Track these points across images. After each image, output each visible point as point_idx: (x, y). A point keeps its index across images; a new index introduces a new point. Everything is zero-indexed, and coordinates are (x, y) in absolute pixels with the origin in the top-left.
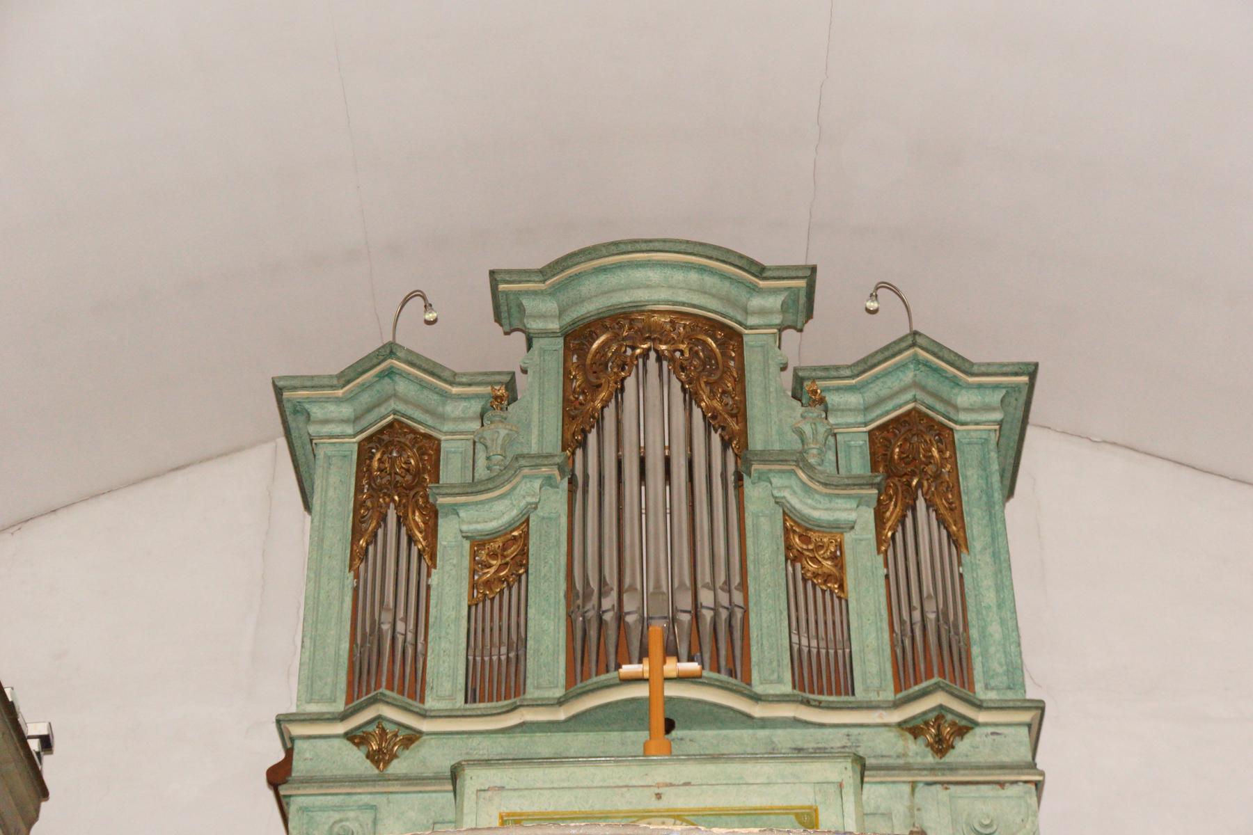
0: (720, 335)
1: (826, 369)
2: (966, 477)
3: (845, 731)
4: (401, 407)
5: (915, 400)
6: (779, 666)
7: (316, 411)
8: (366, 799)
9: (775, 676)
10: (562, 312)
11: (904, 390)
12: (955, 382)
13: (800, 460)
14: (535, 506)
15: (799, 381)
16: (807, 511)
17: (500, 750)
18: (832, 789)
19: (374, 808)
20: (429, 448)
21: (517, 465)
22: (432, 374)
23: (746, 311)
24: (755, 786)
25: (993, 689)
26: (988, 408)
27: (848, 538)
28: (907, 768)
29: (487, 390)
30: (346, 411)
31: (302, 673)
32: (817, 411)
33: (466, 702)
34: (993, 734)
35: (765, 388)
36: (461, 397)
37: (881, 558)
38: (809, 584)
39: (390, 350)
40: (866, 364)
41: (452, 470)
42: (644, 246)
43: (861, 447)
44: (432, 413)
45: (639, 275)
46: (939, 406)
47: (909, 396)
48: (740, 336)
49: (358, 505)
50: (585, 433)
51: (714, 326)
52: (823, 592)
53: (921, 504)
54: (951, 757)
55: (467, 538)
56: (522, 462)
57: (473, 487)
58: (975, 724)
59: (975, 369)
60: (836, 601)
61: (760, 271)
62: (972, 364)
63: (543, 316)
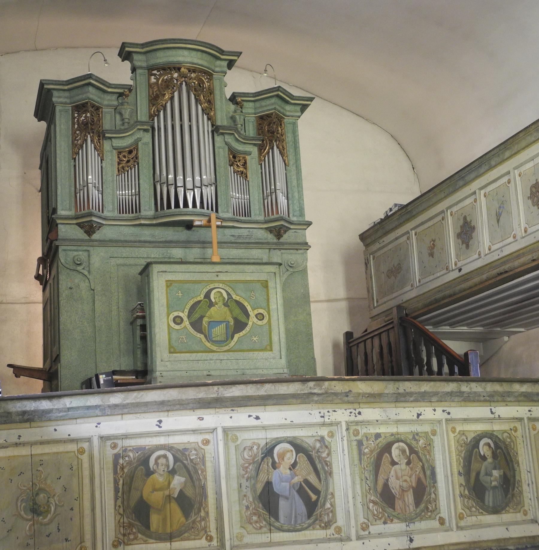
2: (288, 137)
3: (248, 230)
6: (227, 206)
8: (85, 248)
9: (226, 210)
17: (131, 232)
18: (273, 274)
19: (88, 251)
21: (136, 124)
23: (216, 67)
24: (276, 296)
25: (295, 216)
27: (248, 158)
28: (268, 243)
33: (120, 213)
34: (295, 232)
35: (221, 97)
37: (260, 166)
38: (236, 174)
42: (184, 42)
43: (253, 122)
50: (159, 111)
52: (240, 177)
53: (275, 147)
54: (282, 240)
55: (115, 149)
56: (138, 123)
58: (290, 229)
59: (294, 98)
60: (244, 181)
62: (293, 96)
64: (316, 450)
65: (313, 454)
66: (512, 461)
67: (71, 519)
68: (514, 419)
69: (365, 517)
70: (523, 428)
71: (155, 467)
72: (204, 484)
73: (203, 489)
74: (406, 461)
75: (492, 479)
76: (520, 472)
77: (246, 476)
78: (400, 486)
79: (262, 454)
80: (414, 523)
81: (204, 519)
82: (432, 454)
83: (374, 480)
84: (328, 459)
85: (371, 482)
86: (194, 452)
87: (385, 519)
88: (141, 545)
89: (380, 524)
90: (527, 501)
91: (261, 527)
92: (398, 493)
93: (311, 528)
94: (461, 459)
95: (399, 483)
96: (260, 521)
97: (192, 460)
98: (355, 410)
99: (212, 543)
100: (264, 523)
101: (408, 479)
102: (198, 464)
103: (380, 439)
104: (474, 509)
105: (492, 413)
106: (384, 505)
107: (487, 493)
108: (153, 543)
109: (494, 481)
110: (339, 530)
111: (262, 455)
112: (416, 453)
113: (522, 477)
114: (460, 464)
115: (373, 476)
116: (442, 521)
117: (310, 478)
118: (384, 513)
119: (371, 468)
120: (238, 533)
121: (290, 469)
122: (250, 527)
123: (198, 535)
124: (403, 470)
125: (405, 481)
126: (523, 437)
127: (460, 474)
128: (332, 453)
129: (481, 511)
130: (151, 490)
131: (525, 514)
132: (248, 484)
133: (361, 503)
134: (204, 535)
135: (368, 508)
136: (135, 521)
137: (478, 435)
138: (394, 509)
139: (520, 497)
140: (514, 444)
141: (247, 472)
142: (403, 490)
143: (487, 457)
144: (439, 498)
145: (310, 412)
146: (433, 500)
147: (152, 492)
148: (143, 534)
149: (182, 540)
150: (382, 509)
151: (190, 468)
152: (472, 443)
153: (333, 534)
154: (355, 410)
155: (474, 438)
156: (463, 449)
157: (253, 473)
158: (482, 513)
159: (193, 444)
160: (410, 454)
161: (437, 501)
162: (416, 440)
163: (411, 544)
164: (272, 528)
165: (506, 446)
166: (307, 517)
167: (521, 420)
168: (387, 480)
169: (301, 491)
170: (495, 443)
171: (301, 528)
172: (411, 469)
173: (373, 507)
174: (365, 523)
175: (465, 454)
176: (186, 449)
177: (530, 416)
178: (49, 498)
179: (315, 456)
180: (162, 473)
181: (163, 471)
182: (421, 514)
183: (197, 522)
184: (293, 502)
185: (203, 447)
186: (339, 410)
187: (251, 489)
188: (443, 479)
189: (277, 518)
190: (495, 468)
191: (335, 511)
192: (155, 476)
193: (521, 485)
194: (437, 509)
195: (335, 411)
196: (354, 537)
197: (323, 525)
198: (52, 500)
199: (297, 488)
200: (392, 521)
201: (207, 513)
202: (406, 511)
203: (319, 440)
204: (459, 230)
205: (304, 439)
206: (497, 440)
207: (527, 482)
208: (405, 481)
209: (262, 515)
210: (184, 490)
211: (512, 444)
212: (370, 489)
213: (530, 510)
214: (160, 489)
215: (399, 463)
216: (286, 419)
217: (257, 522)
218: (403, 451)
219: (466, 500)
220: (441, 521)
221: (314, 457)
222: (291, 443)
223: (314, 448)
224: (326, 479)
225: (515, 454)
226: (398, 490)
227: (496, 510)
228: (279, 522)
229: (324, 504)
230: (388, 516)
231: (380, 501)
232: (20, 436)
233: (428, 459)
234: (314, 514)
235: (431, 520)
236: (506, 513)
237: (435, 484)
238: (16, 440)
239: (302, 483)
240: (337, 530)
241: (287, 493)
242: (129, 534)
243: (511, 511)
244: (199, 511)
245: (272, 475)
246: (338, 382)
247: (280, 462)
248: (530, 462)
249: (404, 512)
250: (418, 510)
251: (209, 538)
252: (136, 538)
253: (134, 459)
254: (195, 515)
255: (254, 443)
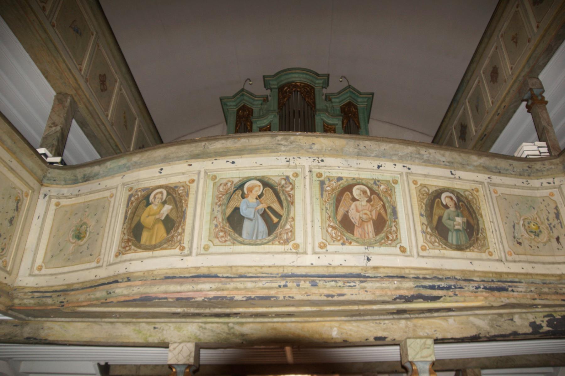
0: (310, 87)
1: (332, 94)
4: (245, 102)
5: (350, 99)
7: (228, 104)
10: (278, 83)
11: (347, 98)
12: (358, 96)
13: (327, 111)
14: (272, 121)
15: (326, 96)
16: (328, 121)
20: (251, 112)
22: (251, 95)
23: (315, 83)
26: (365, 102)
27: (337, 127)
29: (262, 99)
30: (234, 104)
31: (523, 277)
32: (330, 102)
36: (257, 100)
39: (243, 90)
40: (340, 92)
41: (256, 114)
44: (251, 104)
45: (294, 75)
46: (355, 101)
47: (348, 99)
48: (314, 89)
49: (237, 121)
51: (309, 86)
57: (260, 117)
61: (318, 75)
63: (274, 85)
64: (281, 185)
65: (279, 188)
66: (475, 213)
67: (96, 241)
68: (474, 181)
69: (323, 238)
70: (484, 190)
71: (153, 200)
72: (185, 210)
73: (184, 213)
74: (367, 199)
75: (455, 223)
76: (484, 222)
77: (219, 203)
78: (360, 218)
79: (234, 188)
80: (373, 247)
81: (180, 234)
82: (393, 197)
83: (335, 211)
84: (291, 193)
85: (332, 212)
86: (182, 188)
87: (344, 241)
88: (131, 254)
89: (340, 245)
90: (491, 245)
91: (226, 241)
92: (357, 223)
93: (271, 243)
94: (423, 204)
95: (360, 215)
96: (226, 236)
97: (179, 194)
98: (318, 158)
99: (183, 252)
100: (229, 238)
101: (369, 213)
102: (183, 196)
103: (341, 182)
104: (436, 244)
105: (452, 174)
106: (343, 230)
107: (450, 234)
108: (140, 252)
109: (457, 225)
110: (297, 246)
111: (235, 189)
112: (378, 195)
113: (486, 226)
114: (422, 208)
115: (333, 207)
116: (403, 249)
117: (274, 205)
118: (343, 236)
119: (332, 202)
120: (205, 245)
121: (257, 199)
122: (216, 241)
123: (174, 246)
124: (363, 206)
125: (365, 214)
126: (484, 196)
127: (422, 215)
128: (295, 188)
129: (444, 246)
130: (147, 216)
131: (491, 254)
132: (219, 209)
133: (321, 227)
134: (178, 246)
135: (327, 231)
136: (132, 237)
137: (440, 189)
138: (353, 234)
139: (484, 240)
140: (476, 200)
141: (220, 201)
142: (363, 221)
143: (450, 207)
144: (400, 230)
145: (278, 158)
146: (393, 232)
147: (148, 217)
148: (135, 246)
149: (161, 249)
150: (341, 233)
151: (177, 199)
152: (434, 194)
153: (291, 249)
154: (318, 158)
155: (436, 191)
156: (424, 197)
157: (225, 201)
158: (445, 248)
159: (182, 183)
160: (371, 194)
161: (398, 233)
162: (376, 185)
163: (369, 262)
164: (235, 242)
165: (469, 202)
166: (267, 234)
167: (481, 183)
168: (347, 212)
169: (264, 215)
170: (458, 198)
171: (261, 243)
172: (372, 206)
173: (332, 231)
174: (323, 243)
175: (426, 201)
176: (176, 187)
177: (490, 182)
178: (87, 228)
179: (280, 190)
180: (157, 203)
181: (158, 202)
182: (381, 241)
183: (175, 236)
184: (257, 223)
185: (189, 184)
186: (304, 157)
187: (221, 213)
188: (404, 217)
189: (240, 234)
190: (458, 216)
191: (295, 231)
192: (152, 206)
193: (485, 231)
194: (397, 239)
195: (299, 158)
196: (309, 250)
197: (282, 241)
198: (88, 229)
199: (261, 213)
200: (350, 243)
201: (183, 230)
202: (365, 237)
203: (284, 179)
204: (459, 134)
205: (271, 178)
206: (459, 196)
207: (491, 230)
208: (365, 214)
209: (228, 232)
210: (169, 214)
211: (474, 200)
212: (330, 217)
213: (495, 252)
214: (154, 215)
215: (360, 200)
216: (256, 163)
217: (222, 237)
218: (364, 192)
219: (428, 236)
220: (402, 249)
221: (279, 190)
222: (260, 180)
223: (280, 184)
224: (288, 207)
225: (478, 208)
226: (358, 220)
227: (459, 248)
228: (242, 237)
229: (285, 225)
230: (347, 239)
231: (340, 227)
232: (79, 190)
233: (390, 201)
234: (275, 232)
235: (391, 247)
236: (470, 251)
237: (397, 220)
238: (77, 193)
239: (266, 209)
240: (295, 246)
241: (252, 216)
242: (127, 246)
243: (476, 250)
244: (178, 228)
245: (240, 203)
246: (303, 137)
247: (249, 194)
248: (492, 214)
249: (363, 237)
250: (378, 238)
251: (181, 248)
252: (130, 249)
253: (141, 196)
254: (174, 231)
255: (229, 181)
